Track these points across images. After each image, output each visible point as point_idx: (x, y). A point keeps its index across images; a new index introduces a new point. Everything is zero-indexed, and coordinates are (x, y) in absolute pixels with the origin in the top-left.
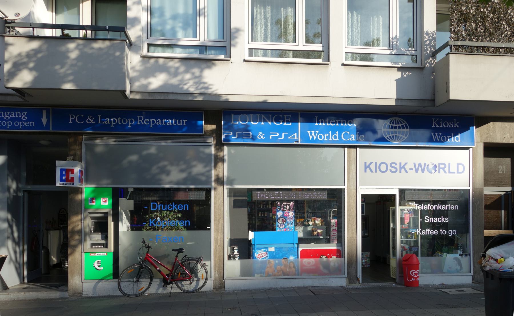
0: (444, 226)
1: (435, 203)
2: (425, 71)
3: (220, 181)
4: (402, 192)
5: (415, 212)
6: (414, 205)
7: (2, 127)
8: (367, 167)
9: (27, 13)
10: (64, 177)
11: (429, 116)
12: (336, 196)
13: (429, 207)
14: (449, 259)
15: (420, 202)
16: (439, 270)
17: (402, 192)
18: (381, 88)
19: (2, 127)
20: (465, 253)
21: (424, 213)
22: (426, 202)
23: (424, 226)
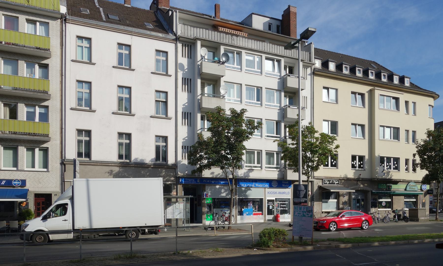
0: (285, 207)
1: (283, 201)
2: (283, 174)
3: (421, 190)
4: (276, 199)
5: (278, 204)
6: (278, 202)
7: (12, 54)
8: (268, 193)
9: (287, 7)
10: (334, 163)
11: (281, 183)
12: (261, 200)
13: (282, 203)
14: (286, 215)
15: (280, 201)
16: (284, 218)
17: (276, 199)
18: (274, 175)
19: (12, 54)
20: (290, 214)
21: (281, 204)
22: (281, 201)
23: (281, 207)
